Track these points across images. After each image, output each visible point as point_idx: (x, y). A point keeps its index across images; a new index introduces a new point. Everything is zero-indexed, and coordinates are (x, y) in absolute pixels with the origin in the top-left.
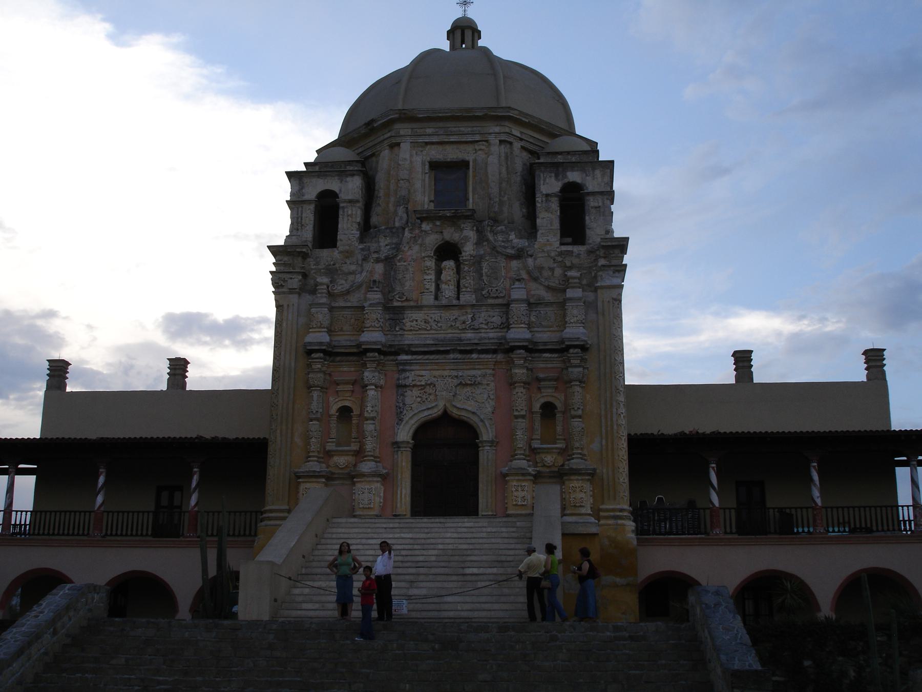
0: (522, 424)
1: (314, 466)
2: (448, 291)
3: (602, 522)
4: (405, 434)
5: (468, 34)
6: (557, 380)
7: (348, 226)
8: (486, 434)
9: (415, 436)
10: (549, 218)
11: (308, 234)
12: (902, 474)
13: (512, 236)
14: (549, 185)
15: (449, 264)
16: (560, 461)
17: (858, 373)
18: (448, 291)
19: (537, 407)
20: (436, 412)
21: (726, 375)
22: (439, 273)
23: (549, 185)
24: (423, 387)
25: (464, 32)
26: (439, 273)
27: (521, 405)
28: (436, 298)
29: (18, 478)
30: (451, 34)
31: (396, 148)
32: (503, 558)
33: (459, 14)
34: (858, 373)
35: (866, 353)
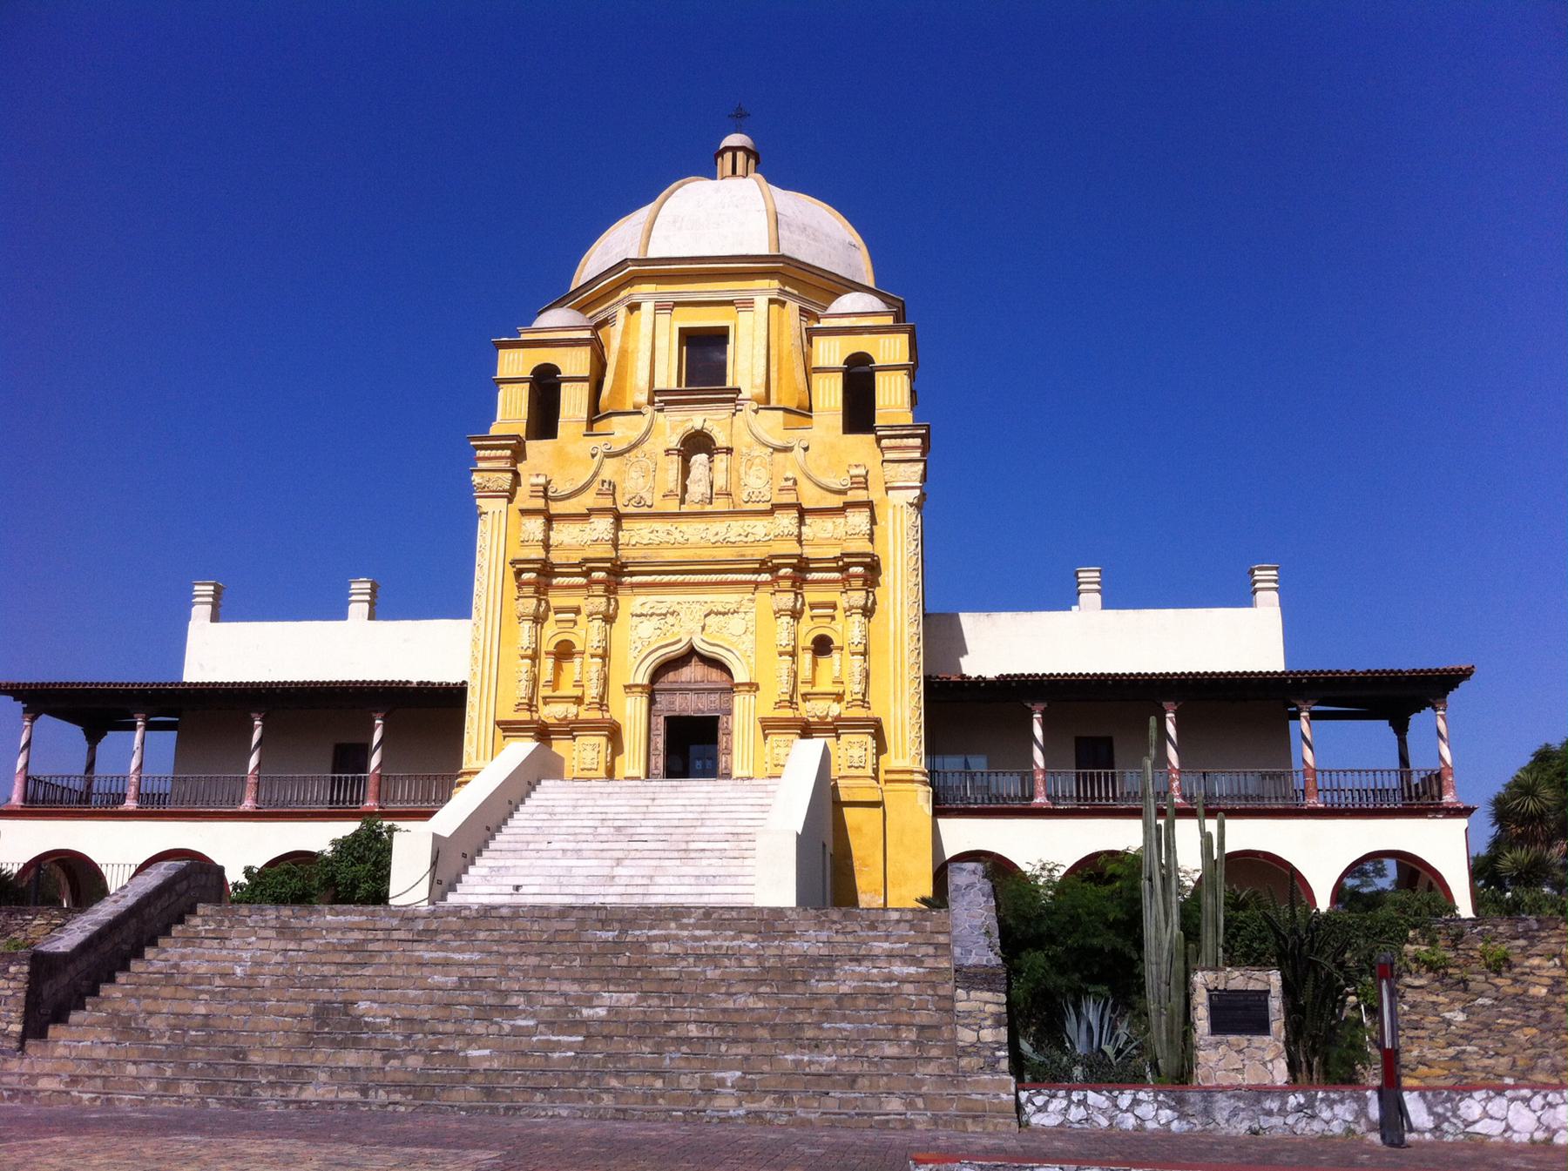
2: (697, 489)
7: (573, 401)
10: (830, 395)
26: (686, 471)
28: (682, 501)
32: (741, 830)
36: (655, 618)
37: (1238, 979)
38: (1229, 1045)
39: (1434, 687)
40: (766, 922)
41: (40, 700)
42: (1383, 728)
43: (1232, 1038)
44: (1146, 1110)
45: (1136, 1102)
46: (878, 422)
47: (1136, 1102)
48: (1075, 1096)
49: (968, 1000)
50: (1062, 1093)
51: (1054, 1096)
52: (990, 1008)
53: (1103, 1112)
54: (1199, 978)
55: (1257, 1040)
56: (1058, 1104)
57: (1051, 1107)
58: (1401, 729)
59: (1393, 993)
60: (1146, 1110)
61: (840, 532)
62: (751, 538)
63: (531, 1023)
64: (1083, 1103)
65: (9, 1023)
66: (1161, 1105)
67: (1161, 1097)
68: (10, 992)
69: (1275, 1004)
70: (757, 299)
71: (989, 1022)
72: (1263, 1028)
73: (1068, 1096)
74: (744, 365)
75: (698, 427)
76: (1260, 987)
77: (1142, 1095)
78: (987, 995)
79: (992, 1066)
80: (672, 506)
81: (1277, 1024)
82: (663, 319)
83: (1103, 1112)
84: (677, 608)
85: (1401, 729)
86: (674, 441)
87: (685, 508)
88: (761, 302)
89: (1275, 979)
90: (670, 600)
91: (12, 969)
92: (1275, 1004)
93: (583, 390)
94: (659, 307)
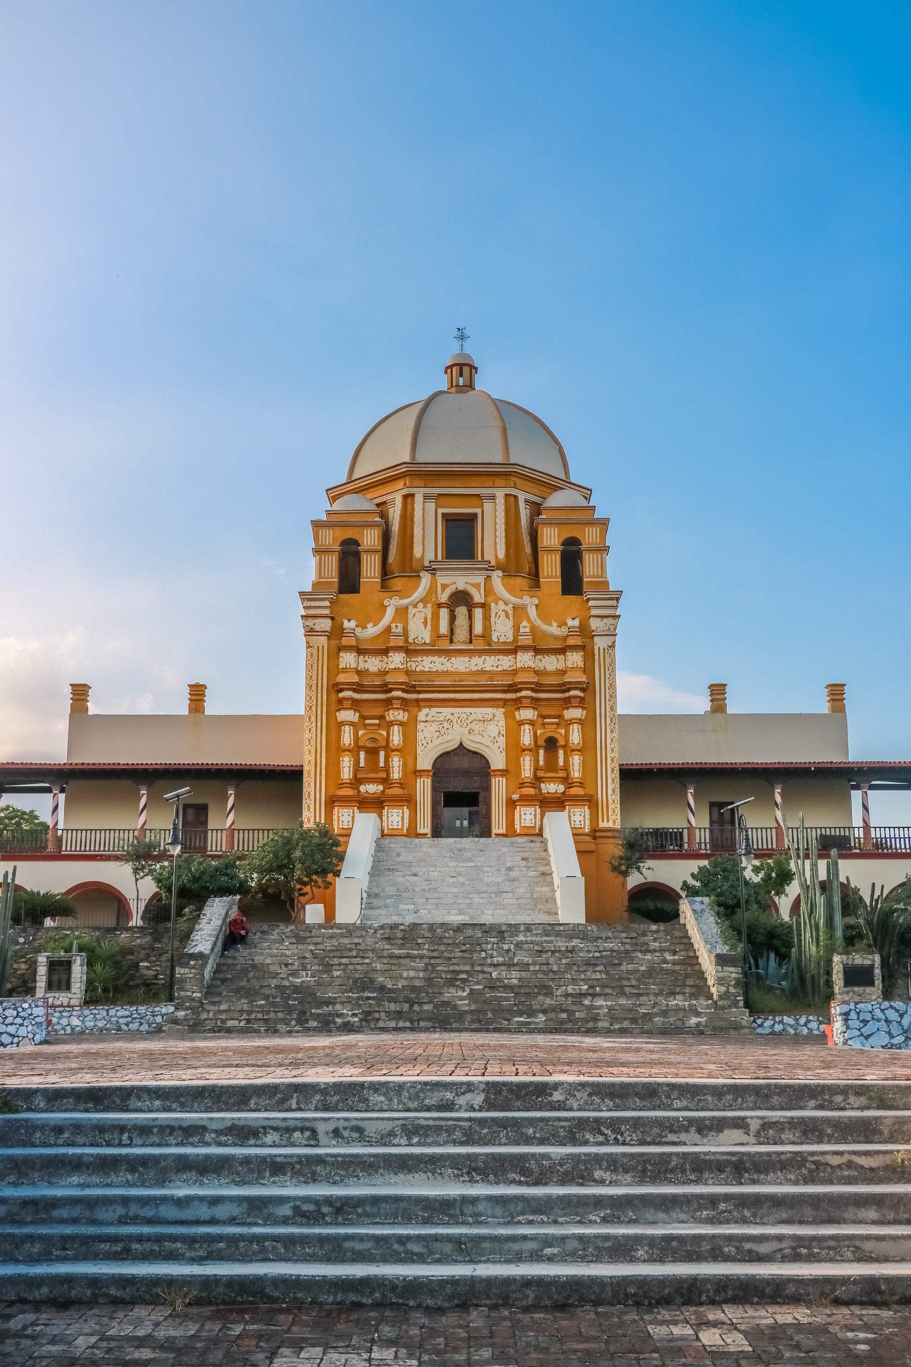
2: (461, 634)
3: (598, 841)
5: (466, 370)
7: (370, 567)
8: (498, 761)
12: (856, 796)
14: (551, 538)
16: (561, 788)
19: (541, 742)
20: (453, 745)
22: (453, 618)
23: (551, 538)
25: (463, 372)
27: (527, 739)
28: (451, 641)
31: (409, 500)
36: (434, 724)
37: (859, 959)
38: (854, 992)
40: (574, 932)
43: (856, 989)
45: (808, 1021)
47: (808, 1021)
48: (777, 1019)
49: (723, 971)
50: (771, 1018)
51: (767, 1019)
52: (733, 975)
53: (791, 1026)
54: (836, 958)
55: (868, 990)
56: (768, 1023)
57: (765, 1025)
59: (327, 1304)
60: (813, 1025)
61: (561, 666)
62: (500, 668)
63: (480, 987)
64: (781, 1022)
65: (193, 993)
66: (820, 1023)
67: (821, 1019)
68: (191, 976)
69: (877, 971)
70: (497, 494)
71: (733, 983)
72: (871, 983)
73: (774, 1019)
74: (493, 541)
75: (461, 588)
76: (869, 962)
77: (811, 1018)
78: (732, 969)
79: (735, 1004)
81: (878, 982)
83: (791, 1026)
84: (451, 717)
89: (877, 958)
91: (192, 963)
92: (877, 971)
93: (376, 559)
94: (426, 497)
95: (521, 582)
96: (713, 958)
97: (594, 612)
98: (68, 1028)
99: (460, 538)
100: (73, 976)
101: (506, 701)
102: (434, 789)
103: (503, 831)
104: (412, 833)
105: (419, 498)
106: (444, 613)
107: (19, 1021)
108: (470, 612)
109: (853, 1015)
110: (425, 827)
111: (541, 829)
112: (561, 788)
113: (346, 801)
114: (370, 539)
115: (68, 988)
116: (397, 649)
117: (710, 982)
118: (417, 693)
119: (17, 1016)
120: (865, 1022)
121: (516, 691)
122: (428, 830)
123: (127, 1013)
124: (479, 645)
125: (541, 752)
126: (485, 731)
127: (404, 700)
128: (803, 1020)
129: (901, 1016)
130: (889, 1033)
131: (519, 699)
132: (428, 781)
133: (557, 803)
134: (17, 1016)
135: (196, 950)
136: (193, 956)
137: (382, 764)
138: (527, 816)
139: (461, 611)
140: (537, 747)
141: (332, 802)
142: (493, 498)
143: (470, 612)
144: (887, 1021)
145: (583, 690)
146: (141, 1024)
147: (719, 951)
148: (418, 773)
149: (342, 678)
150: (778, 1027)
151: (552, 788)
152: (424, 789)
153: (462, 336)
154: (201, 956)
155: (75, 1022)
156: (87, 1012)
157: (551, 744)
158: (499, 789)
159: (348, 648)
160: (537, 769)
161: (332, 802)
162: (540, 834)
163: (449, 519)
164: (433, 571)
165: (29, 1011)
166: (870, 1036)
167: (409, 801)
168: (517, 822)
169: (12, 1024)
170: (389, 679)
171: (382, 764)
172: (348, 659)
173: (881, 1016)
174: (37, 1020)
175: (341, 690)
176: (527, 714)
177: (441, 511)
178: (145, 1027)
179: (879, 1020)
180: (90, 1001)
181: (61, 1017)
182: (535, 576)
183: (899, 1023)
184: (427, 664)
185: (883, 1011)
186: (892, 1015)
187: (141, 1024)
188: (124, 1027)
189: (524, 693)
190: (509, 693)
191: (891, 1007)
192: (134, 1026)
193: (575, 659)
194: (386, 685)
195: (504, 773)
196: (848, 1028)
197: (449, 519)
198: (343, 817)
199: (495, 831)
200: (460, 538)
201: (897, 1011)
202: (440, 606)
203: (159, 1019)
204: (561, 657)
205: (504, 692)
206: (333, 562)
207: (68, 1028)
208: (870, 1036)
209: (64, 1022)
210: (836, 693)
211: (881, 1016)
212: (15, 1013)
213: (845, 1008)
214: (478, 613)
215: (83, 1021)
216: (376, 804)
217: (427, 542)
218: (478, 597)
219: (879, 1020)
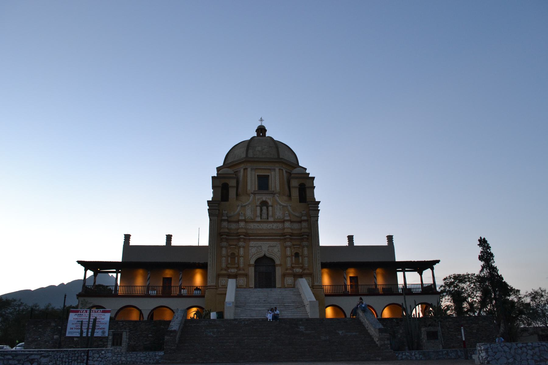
0: (289, 259)
1: (224, 272)
2: (264, 216)
4: (252, 262)
6: (299, 245)
7: (232, 193)
8: (277, 262)
9: (255, 263)
10: (295, 193)
11: (219, 198)
12: (400, 275)
13: (516, 300)
14: (295, 183)
15: (264, 208)
17: (385, 243)
18: (264, 216)
19: (293, 254)
20: (262, 255)
21: (345, 243)
22: (261, 210)
24: (258, 247)
25: (261, 130)
27: (288, 252)
29: (406, 273)
30: (257, 131)
33: (260, 124)
34: (385, 243)
35: (387, 236)
39: (430, 265)
41: (87, 265)
42: (416, 274)
44: (417, 356)
46: (308, 200)
47: (415, 354)
58: (421, 274)
78: (385, 334)
80: (258, 219)
82: (253, 172)
85: (421, 274)
86: (258, 203)
87: (262, 220)
88: (277, 170)
90: (259, 243)
94: (252, 169)
95: (285, 198)
96: (377, 330)
97: (311, 208)
98: (120, 362)
99: (263, 183)
100: (123, 339)
101: (280, 239)
102: (255, 271)
103: (280, 286)
104: (247, 287)
105: (249, 170)
106: (258, 208)
107: (100, 359)
108: (267, 208)
109: (490, 350)
110: (252, 284)
111: (294, 285)
112: (301, 271)
113: (223, 275)
114: (232, 183)
115: (121, 345)
116: (242, 221)
117: (376, 339)
118: (248, 236)
119: (99, 357)
120: (496, 353)
121: (284, 236)
122: (253, 286)
123: (144, 355)
124: (271, 219)
125: (294, 257)
126: (273, 249)
127: (244, 239)
128: (413, 354)
129: (510, 349)
130: (506, 357)
131: (285, 239)
132: (253, 268)
133: (301, 276)
134: (99, 357)
135: (173, 329)
136: (171, 332)
137: (236, 262)
138: (289, 280)
139: (264, 208)
140: (292, 256)
141: (219, 276)
142: (274, 170)
143: (267, 208)
144: (504, 352)
145: (308, 236)
146: (150, 360)
147: (378, 327)
148: (250, 265)
149: (222, 231)
150: (404, 357)
151: (298, 270)
152: (251, 271)
153: (261, 120)
154: (175, 331)
155: (123, 359)
156: (128, 355)
157: (297, 255)
158: (279, 272)
159: (225, 220)
160: (292, 264)
161: (219, 276)
162: (294, 287)
163: (259, 177)
164: (254, 194)
165: (105, 355)
166: (499, 359)
167: (246, 275)
168: (285, 283)
169: (97, 361)
170: (239, 231)
171: (236, 262)
172: (225, 224)
173: (501, 349)
174: (108, 359)
175: (222, 235)
176: (289, 244)
177: (257, 174)
178: (152, 361)
179: (501, 351)
180: (132, 349)
181: (118, 357)
182: (290, 196)
183: (510, 352)
184: (252, 226)
185: (502, 347)
186: (507, 349)
187: (150, 360)
188: (143, 361)
189: (287, 236)
190: (282, 237)
191: (505, 345)
192: (147, 361)
193: (304, 224)
194: (238, 233)
195: (280, 265)
196: (488, 356)
197: (259, 177)
198: (222, 281)
199: (277, 286)
200: (263, 183)
201: (508, 347)
202: (257, 206)
203: (158, 358)
204: (299, 224)
205: (280, 236)
206: (219, 190)
207: (120, 362)
208: (499, 359)
209: (119, 359)
210: (390, 238)
211: (501, 349)
212: (98, 356)
213: (486, 347)
214: (270, 208)
215: (126, 359)
216: (235, 276)
217: (252, 184)
218: (270, 203)
219: (501, 351)
